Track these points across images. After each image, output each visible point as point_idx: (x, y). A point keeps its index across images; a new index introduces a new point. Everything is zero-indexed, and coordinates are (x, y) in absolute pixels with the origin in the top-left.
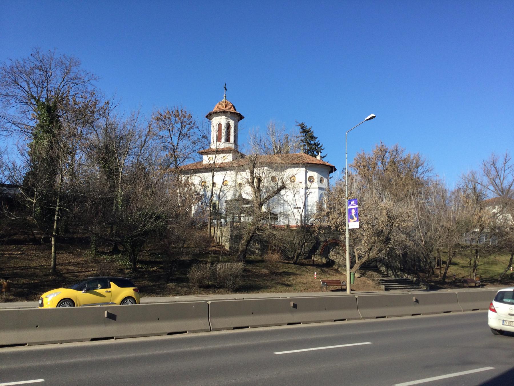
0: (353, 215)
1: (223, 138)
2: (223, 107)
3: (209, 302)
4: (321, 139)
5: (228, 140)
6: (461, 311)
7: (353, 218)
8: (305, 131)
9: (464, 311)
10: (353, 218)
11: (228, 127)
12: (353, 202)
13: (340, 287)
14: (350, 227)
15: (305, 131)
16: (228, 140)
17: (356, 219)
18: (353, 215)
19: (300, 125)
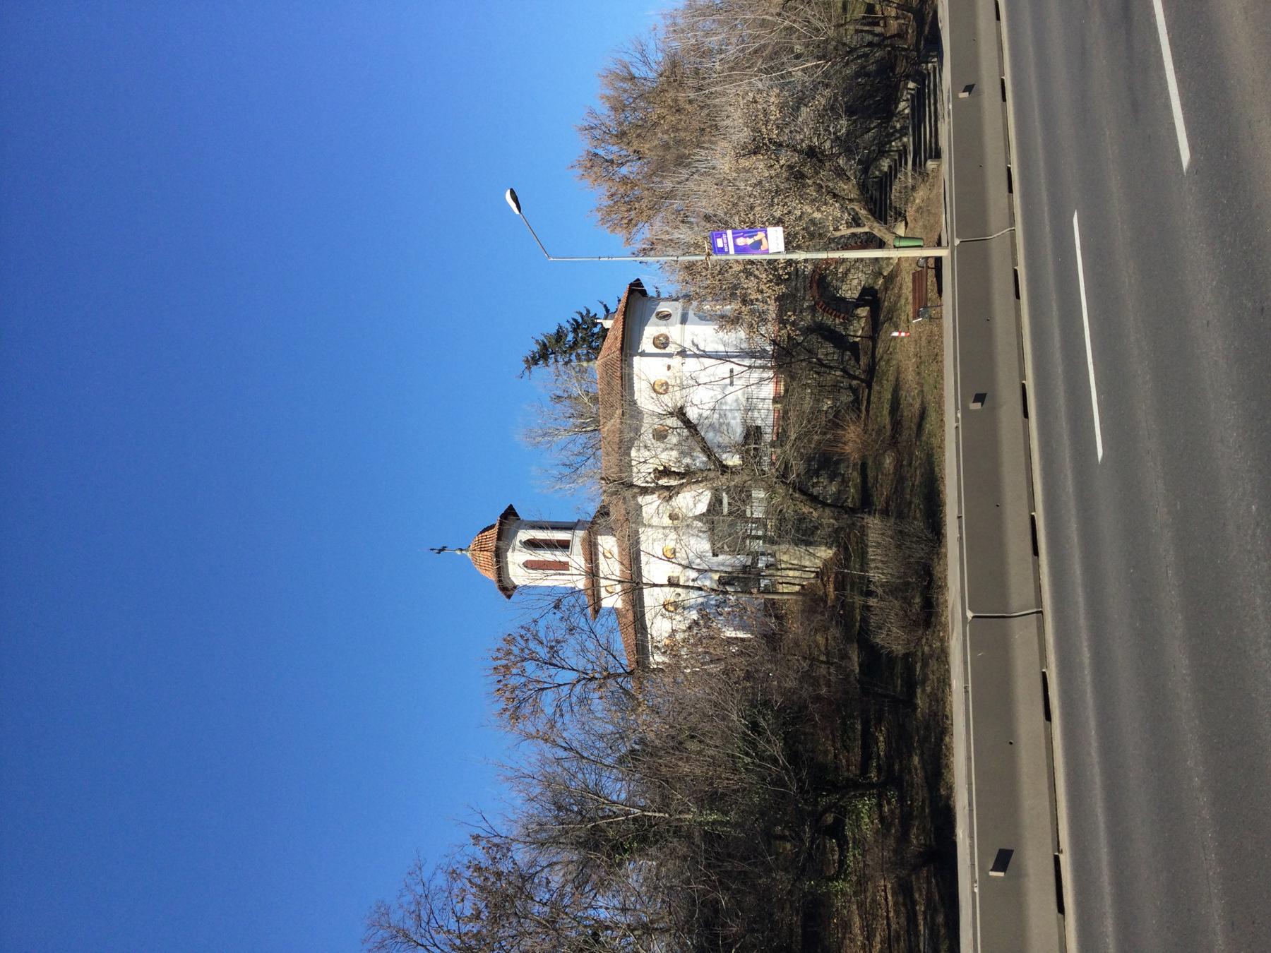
0: (750, 241)
1: (559, 556)
2: (486, 557)
3: (970, 615)
4: (562, 316)
5: (565, 545)
6: (1013, 233)
7: (759, 243)
8: (543, 354)
9: (1012, 222)
10: (759, 243)
11: (532, 544)
12: (720, 243)
13: (931, 273)
14: (782, 248)
15: (543, 354)
16: (565, 545)
17: (760, 235)
18: (750, 241)
19: (529, 368)
